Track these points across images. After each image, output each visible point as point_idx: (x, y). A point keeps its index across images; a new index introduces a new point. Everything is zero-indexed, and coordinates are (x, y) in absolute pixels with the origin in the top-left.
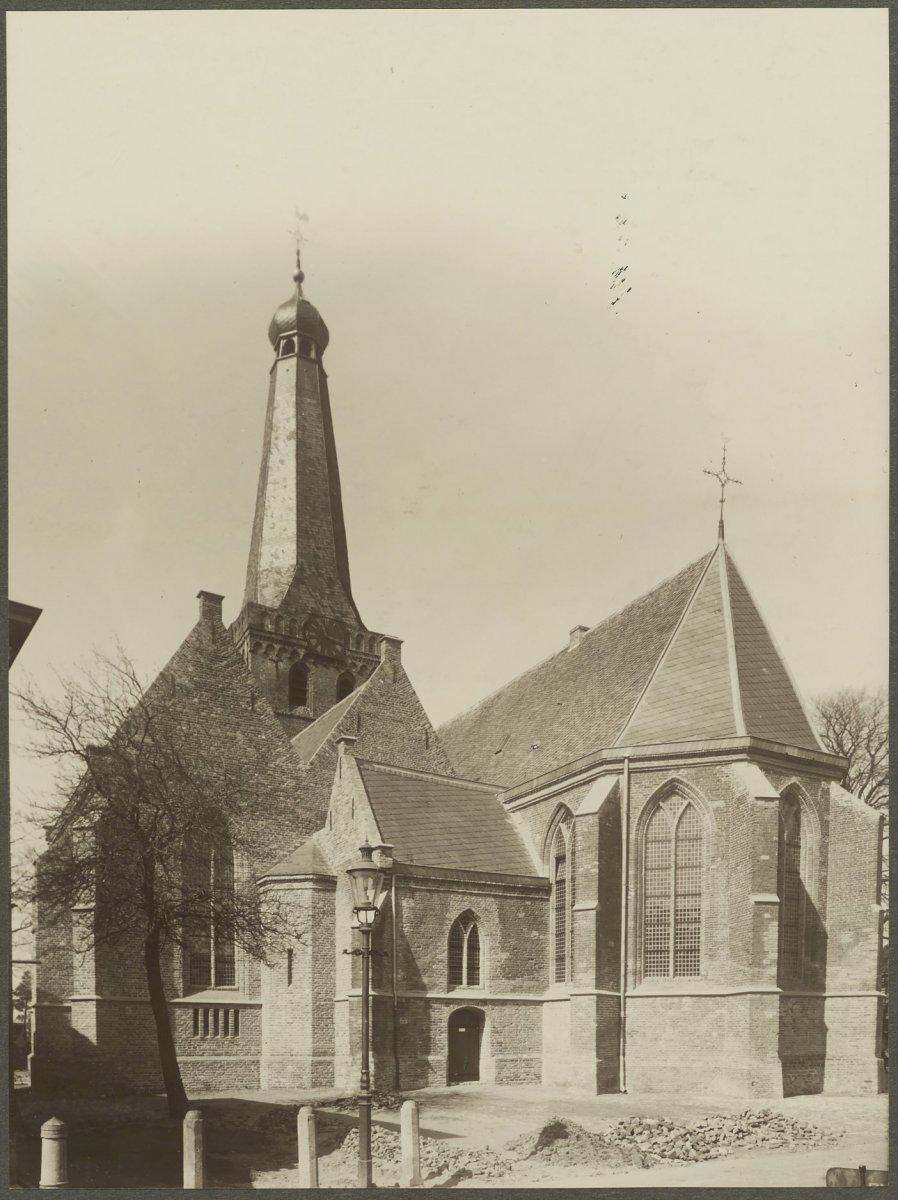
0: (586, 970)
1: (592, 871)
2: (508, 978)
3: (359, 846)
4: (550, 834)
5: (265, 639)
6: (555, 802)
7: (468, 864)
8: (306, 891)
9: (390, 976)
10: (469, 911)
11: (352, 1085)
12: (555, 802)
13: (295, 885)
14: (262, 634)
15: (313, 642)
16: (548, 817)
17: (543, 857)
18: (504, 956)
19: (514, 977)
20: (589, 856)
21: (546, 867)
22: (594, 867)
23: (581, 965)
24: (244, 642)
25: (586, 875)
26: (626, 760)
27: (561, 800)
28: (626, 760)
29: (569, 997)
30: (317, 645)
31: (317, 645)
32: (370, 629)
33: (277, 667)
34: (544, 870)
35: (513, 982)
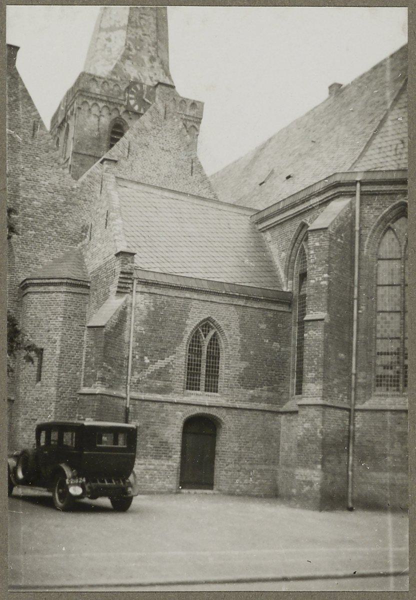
0: (314, 381)
1: (322, 283)
2: (246, 388)
3: (114, 253)
4: (294, 251)
5: (92, 98)
6: (298, 222)
7: (212, 275)
8: (60, 294)
9: (125, 377)
10: (209, 319)
11: (391, 549)
12: (298, 222)
13: (52, 288)
14: (89, 95)
15: (132, 102)
16: (291, 236)
17: (287, 273)
18: (244, 365)
19: (253, 387)
20: (320, 269)
21: (290, 282)
22: (324, 279)
23: (310, 375)
24: (74, 102)
25: (317, 287)
26: (358, 185)
27: (303, 220)
28: (358, 185)
29: (297, 408)
30: (134, 105)
31: (134, 105)
32: (181, 95)
33: (99, 120)
34: (288, 286)
35: (251, 391)
